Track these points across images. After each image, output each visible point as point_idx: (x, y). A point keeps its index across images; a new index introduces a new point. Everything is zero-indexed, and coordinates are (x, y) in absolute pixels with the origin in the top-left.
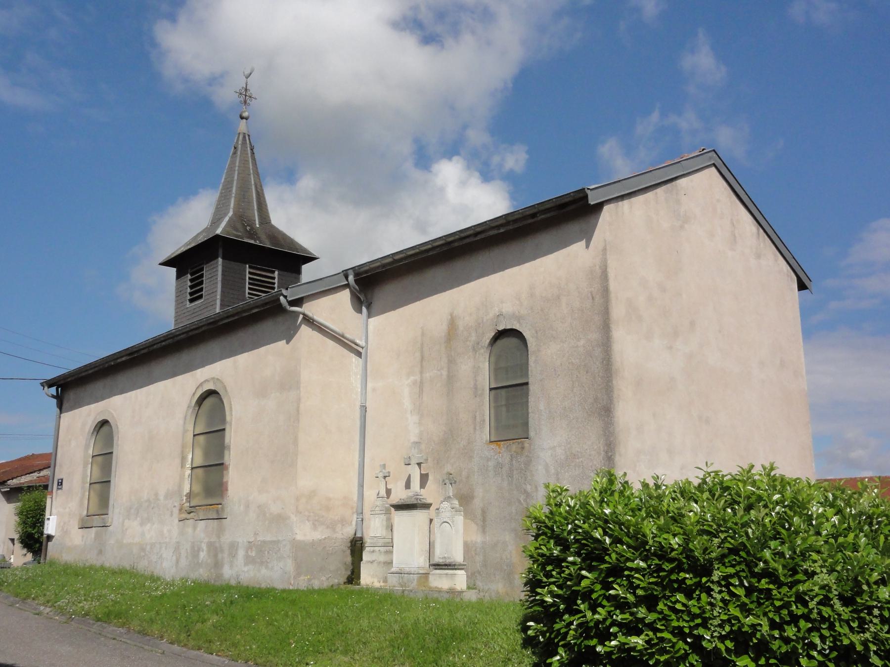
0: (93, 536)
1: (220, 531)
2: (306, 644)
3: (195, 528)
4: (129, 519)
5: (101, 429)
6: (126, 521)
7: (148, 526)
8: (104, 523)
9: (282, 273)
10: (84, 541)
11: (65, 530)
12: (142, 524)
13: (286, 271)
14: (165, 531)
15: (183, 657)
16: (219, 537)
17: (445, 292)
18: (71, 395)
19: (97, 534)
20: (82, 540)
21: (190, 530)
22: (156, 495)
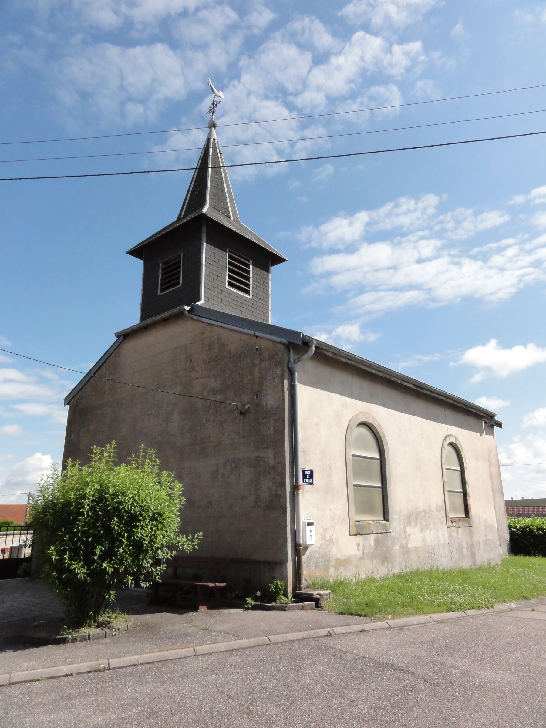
0: (372, 543)
1: (471, 534)
2: (272, 667)
3: (457, 532)
4: (410, 526)
5: (123, 342)
6: (408, 528)
7: (427, 532)
8: (386, 529)
9: (254, 267)
10: (361, 550)
11: (328, 538)
12: (422, 530)
13: (216, 246)
14: (440, 535)
15: (543, 571)
16: (471, 538)
17: (323, 390)
18: (492, 416)
19: (377, 541)
20: (358, 550)
21: (454, 534)
22: (430, 507)
